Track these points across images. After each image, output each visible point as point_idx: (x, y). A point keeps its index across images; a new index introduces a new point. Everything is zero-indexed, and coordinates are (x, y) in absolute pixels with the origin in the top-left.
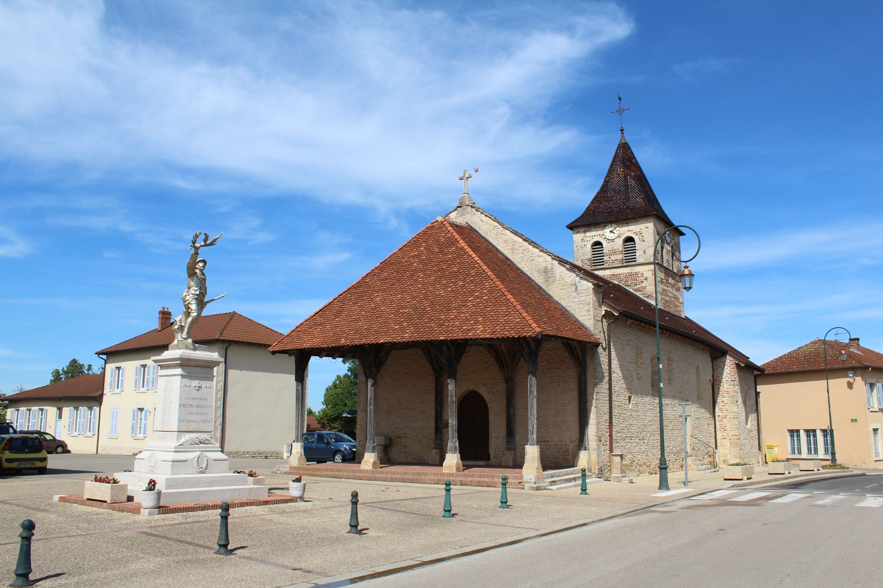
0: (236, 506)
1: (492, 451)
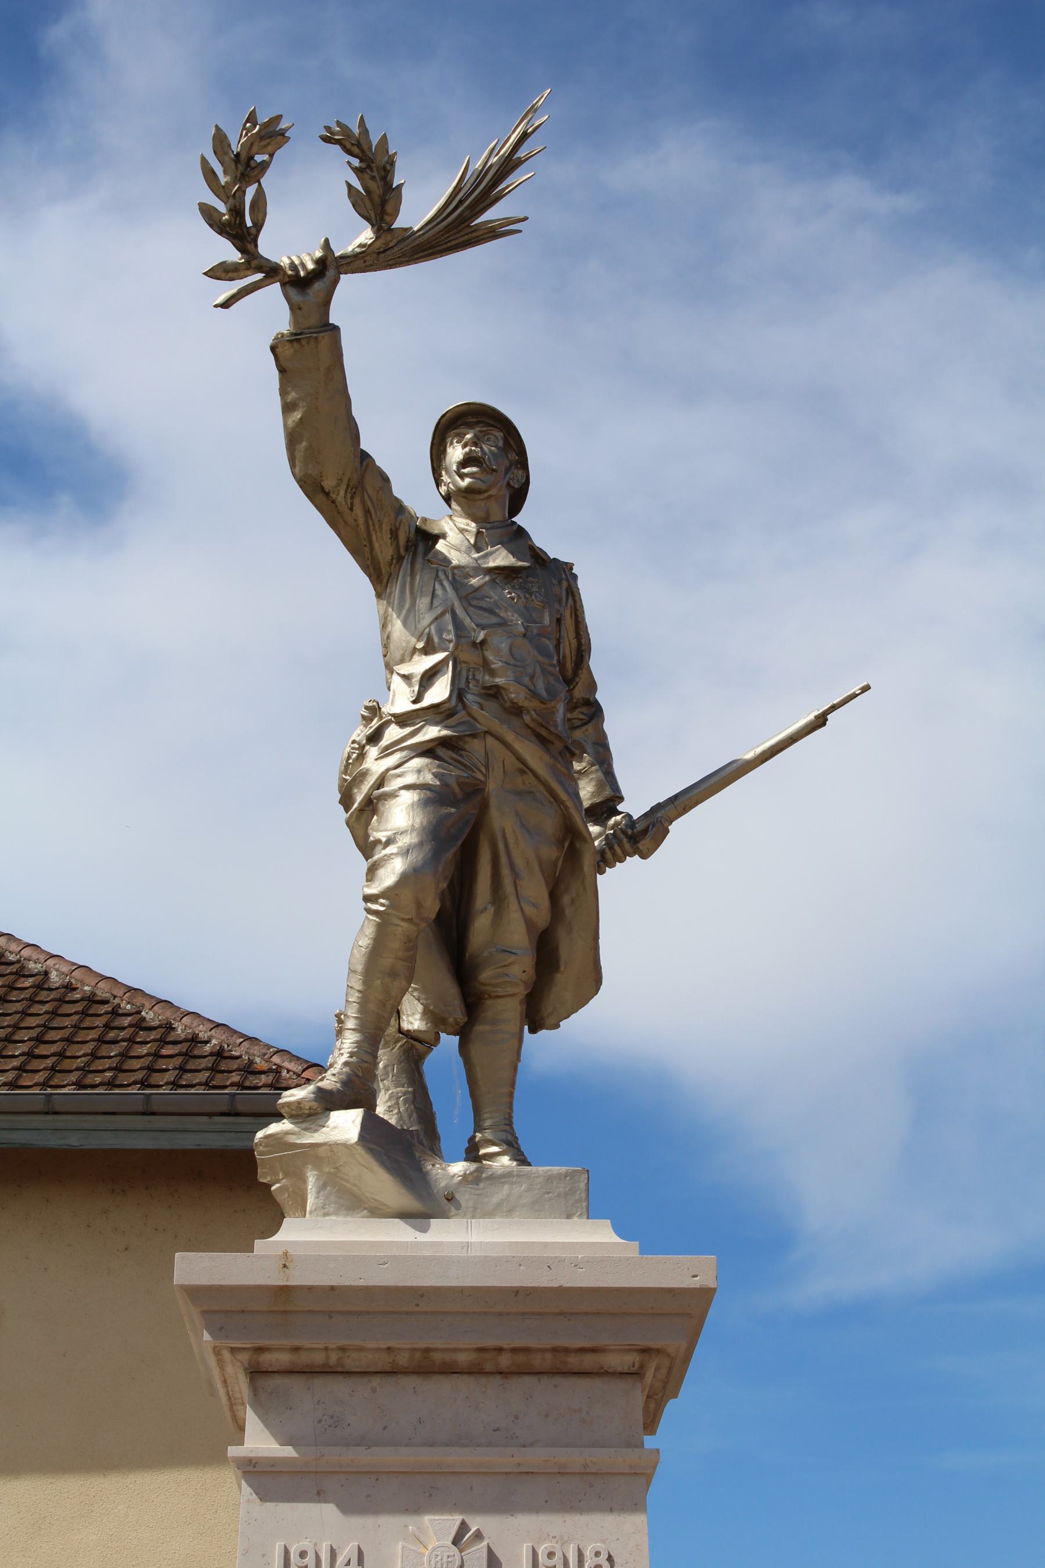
1: (696, 1283)
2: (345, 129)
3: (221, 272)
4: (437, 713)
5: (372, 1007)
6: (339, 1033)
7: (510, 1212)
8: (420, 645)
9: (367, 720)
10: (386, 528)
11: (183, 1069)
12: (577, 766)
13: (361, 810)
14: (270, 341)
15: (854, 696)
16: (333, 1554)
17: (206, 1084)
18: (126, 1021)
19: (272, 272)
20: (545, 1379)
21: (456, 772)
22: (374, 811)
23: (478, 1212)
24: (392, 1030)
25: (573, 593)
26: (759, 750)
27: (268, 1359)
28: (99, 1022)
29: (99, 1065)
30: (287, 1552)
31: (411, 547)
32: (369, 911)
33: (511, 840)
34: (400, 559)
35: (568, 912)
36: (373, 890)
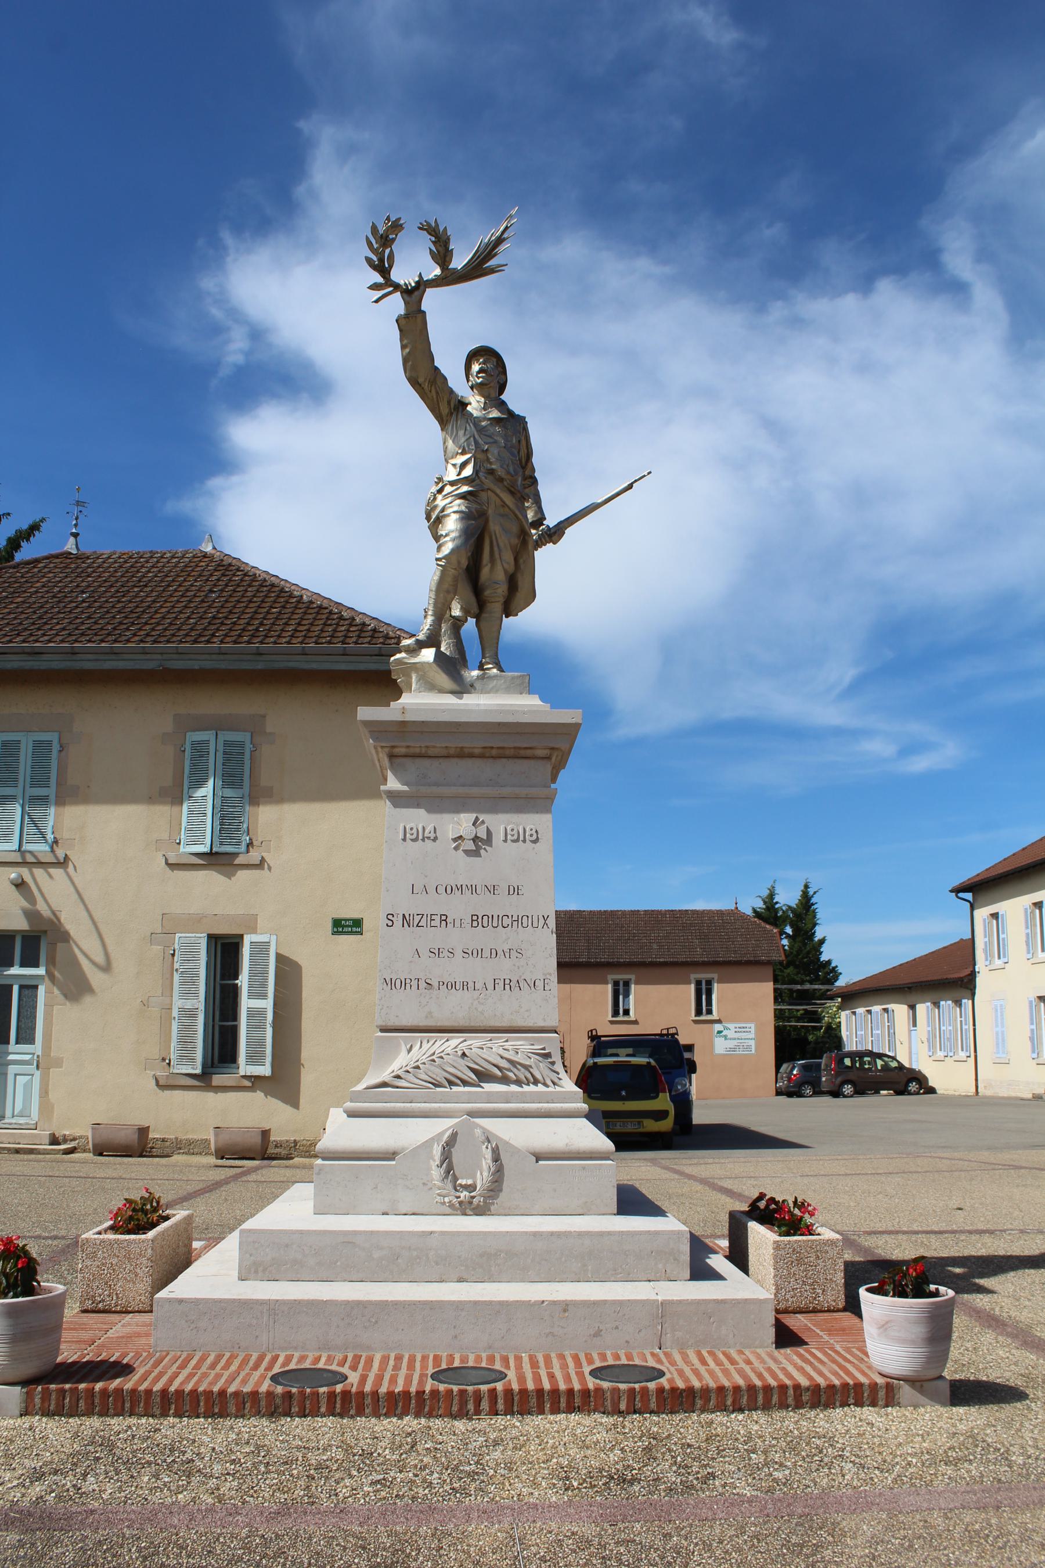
0: (485, 1405)
1: (574, 721)
2: (428, 224)
3: (375, 287)
4: (466, 481)
5: (439, 606)
6: (425, 617)
7: (497, 691)
8: (460, 451)
9: (437, 483)
10: (446, 400)
11: (359, 637)
12: (526, 504)
13: (435, 522)
14: (396, 317)
15: (644, 476)
16: (424, 829)
17: (369, 643)
18: (335, 616)
19: (397, 287)
20: (510, 760)
21: (475, 506)
22: (440, 522)
23: (484, 691)
24: (447, 615)
25: (525, 429)
26: (604, 499)
27: (396, 751)
28: (324, 617)
29: (324, 635)
30: (405, 828)
31: (456, 409)
32: (438, 565)
33: (498, 535)
34: (452, 414)
35: (522, 566)
36: (440, 556)
